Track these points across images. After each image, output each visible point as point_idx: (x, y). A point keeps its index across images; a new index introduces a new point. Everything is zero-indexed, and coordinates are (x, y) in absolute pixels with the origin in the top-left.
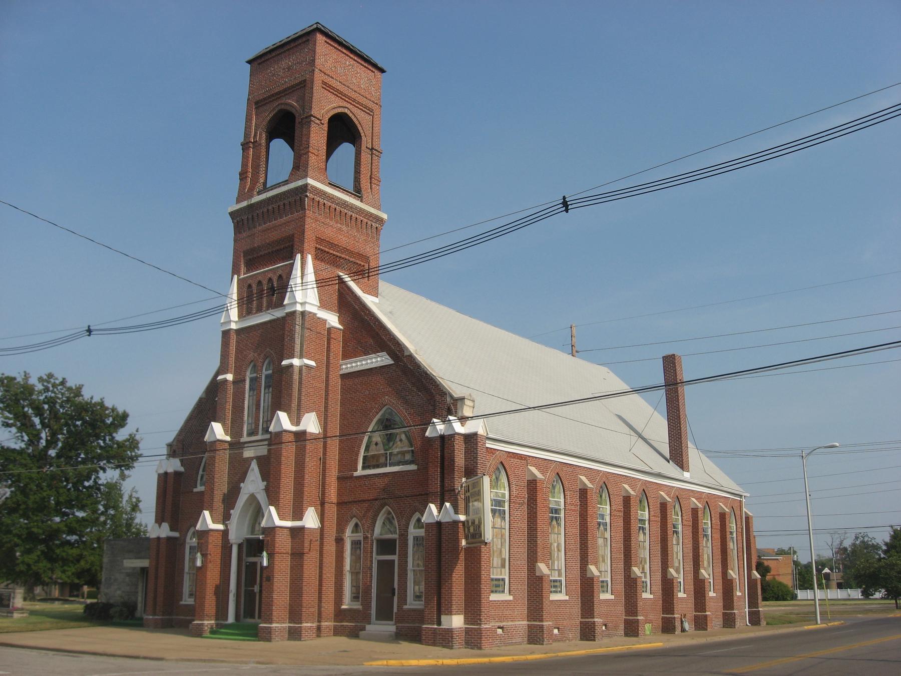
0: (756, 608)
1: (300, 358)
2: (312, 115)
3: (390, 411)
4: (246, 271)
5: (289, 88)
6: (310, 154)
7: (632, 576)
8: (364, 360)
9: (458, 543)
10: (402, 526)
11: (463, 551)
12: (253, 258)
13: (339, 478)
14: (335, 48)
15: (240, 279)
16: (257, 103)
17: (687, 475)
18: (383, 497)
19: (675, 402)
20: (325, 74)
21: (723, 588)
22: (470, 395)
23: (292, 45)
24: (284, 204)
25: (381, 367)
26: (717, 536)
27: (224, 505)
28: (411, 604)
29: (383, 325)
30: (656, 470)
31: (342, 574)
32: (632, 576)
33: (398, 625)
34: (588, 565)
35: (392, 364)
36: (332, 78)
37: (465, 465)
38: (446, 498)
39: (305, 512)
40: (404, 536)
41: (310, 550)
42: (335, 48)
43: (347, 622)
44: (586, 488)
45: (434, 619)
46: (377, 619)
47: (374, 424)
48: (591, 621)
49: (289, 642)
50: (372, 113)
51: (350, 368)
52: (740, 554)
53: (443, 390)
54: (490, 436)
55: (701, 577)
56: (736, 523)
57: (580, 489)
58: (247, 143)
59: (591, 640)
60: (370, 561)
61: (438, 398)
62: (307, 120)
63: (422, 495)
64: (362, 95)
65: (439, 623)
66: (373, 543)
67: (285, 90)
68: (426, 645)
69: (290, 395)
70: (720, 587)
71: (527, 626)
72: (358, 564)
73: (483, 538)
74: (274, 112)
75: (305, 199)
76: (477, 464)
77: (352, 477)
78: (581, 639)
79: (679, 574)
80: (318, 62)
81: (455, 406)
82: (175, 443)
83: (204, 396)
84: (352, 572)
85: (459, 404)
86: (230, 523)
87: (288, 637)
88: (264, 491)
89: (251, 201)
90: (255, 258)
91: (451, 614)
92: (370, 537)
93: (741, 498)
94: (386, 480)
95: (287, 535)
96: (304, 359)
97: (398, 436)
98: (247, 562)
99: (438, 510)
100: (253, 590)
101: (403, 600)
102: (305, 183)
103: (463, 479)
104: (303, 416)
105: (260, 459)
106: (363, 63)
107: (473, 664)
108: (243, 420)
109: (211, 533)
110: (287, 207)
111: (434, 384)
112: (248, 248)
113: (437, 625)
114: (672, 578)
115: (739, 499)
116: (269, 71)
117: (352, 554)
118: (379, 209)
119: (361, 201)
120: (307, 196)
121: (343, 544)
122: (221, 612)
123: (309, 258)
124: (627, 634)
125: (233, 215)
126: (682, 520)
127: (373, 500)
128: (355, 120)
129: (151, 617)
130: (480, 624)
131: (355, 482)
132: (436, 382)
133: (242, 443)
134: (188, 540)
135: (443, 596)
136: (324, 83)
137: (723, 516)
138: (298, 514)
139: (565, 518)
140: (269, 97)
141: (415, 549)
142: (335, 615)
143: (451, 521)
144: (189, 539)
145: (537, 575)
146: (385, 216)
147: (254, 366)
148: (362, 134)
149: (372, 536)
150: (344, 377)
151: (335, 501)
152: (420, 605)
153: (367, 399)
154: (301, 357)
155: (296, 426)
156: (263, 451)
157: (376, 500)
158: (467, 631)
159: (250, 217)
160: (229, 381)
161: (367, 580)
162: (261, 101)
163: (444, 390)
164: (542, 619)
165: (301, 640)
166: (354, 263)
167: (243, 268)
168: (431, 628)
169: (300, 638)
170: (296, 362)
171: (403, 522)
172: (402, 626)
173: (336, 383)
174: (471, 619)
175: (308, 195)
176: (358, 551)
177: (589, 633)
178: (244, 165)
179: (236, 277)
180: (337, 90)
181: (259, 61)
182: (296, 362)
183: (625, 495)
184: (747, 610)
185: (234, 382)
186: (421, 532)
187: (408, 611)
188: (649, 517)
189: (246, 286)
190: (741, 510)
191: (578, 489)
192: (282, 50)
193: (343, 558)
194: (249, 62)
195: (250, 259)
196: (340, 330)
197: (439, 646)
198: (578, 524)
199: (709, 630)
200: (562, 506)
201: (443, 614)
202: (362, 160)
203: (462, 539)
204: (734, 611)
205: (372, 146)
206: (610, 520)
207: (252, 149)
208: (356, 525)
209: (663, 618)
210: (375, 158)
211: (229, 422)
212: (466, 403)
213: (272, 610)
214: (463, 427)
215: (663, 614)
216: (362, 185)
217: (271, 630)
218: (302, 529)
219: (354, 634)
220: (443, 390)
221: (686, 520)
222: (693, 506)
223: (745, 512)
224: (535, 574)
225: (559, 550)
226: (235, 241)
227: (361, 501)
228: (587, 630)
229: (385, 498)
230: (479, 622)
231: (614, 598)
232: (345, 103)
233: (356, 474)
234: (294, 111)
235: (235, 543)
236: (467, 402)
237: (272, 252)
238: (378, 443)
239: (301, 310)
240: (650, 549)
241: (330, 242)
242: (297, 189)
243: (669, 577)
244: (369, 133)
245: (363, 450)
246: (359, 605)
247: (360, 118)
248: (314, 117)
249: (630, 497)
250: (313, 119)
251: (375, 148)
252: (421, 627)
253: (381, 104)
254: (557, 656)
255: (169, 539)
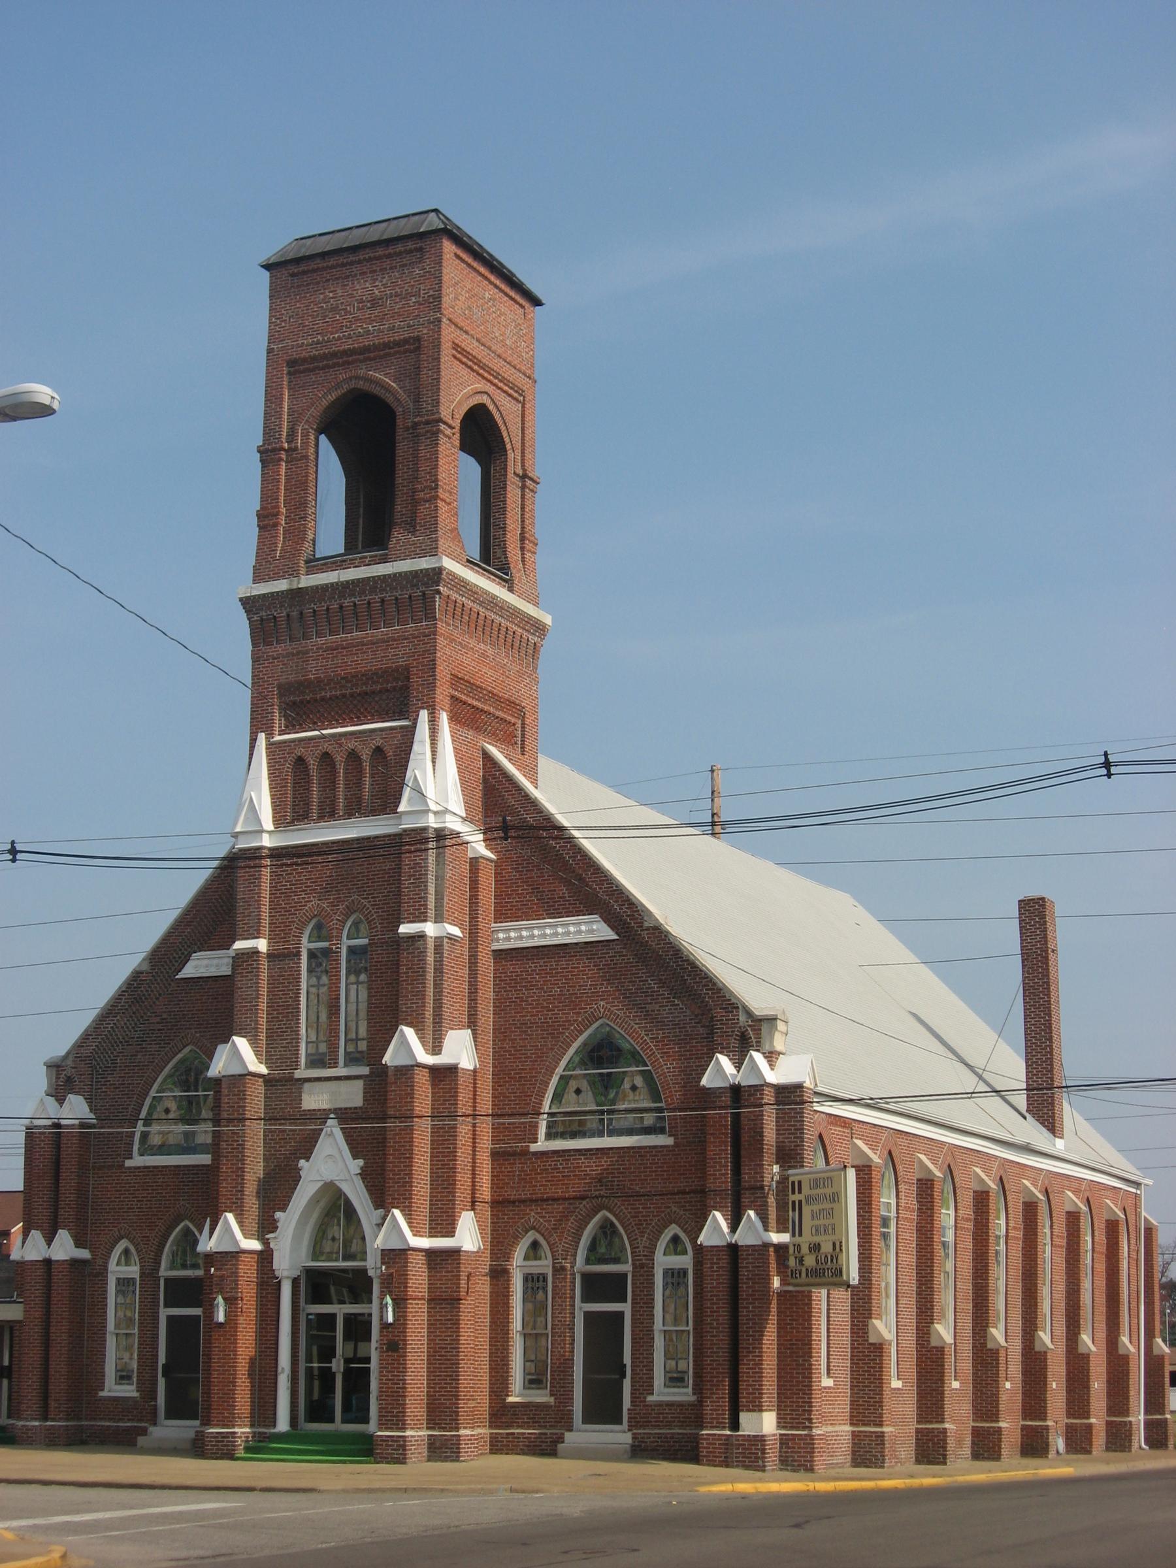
0: (1161, 1414)
1: (435, 922)
2: (440, 420)
3: (608, 1029)
4: (286, 727)
5: (376, 348)
6: (440, 504)
7: (990, 1345)
8: (550, 926)
9: (769, 1283)
10: (641, 1249)
11: (775, 1298)
12: (302, 702)
13: (495, 1155)
14: (469, 265)
15: (272, 744)
16: (292, 363)
17: (1060, 1144)
18: (597, 1193)
19: (1041, 996)
20: (456, 326)
21: (1108, 1373)
22: (784, 1012)
23: (380, 252)
24: (383, 601)
25: (586, 943)
26: (968, 1244)
27: (259, 1201)
28: (661, 1392)
29: (594, 862)
30: (1020, 1139)
31: (508, 1338)
32: (990, 1345)
33: (635, 1431)
34: (933, 1323)
35: (613, 940)
36: (466, 332)
37: (777, 1142)
38: (745, 1201)
39: (458, 1220)
40: (644, 1269)
41: (467, 1293)
42: (469, 265)
43: (519, 1427)
44: (931, 1178)
45: (725, 1419)
46: (585, 1421)
47: (573, 1052)
48: (938, 1429)
49: (430, 1463)
50: (522, 398)
51: (516, 938)
52: (1134, 1304)
53: (725, 996)
54: (820, 1089)
55: (1156, 1352)
56: (956, 1207)
57: (918, 1180)
58: (274, 450)
59: (938, 1463)
60: (570, 1313)
61: (718, 1013)
62: (428, 428)
63: (684, 1192)
64: (508, 363)
65: (735, 1425)
66: (575, 1279)
67: (366, 349)
68: (708, 1465)
69: (422, 995)
70: (911, 1364)
71: (850, 1433)
72: (541, 1319)
73: (845, 1277)
74: (339, 392)
75: (435, 597)
76: (803, 1141)
77: (525, 1152)
78: (918, 1461)
79: (1090, 1342)
80: (446, 301)
81: (758, 1032)
82: (69, 1062)
83: (145, 967)
84: (525, 1335)
85: (765, 1028)
86: (275, 1238)
87: (429, 1456)
88: (359, 1177)
89: (299, 583)
90: (309, 702)
91: (761, 1411)
92: (569, 1268)
93: (1137, 1189)
94: (605, 1162)
95: (422, 1264)
96: (446, 925)
97: (626, 1080)
98: (308, 1314)
99: (728, 1223)
100: (331, 1367)
101: (644, 1384)
102: (437, 565)
103: (775, 1166)
104: (446, 1035)
105: (344, 1115)
106: (507, 290)
107: (825, 1492)
108: (299, 1035)
109: (243, 1257)
110: (392, 609)
111: (710, 987)
112: (292, 678)
113: (729, 1430)
114: (1043, 1350)
115: (1134, 1190)
116: (322, 296)
117: (524, 1300)
118: (536, 604)
119: (511, 590)
120: (438, 592)
121: (509, 1281)
122: (263, 1411)
123: (444, 718)
124: (976, 1456)
125: (249, 604)
126: (1052, 1235)
127: (575, 1198)
128: (497, 416)
129: (37, 1423)
130: (810, 1428)
131: (533, 1163)
132: (714, 984)
133: (299, 1080)
134: (112, 1265)
135: (743, 1377)
136: (456, 346)
137: (926, 1187)
138: (444, 1224)
139: (897, 1235)
140: (324, 357)
141: (668, 1292)
142: (492, 1415)
143: (760, 1243)
144: (115, 1263)
145: (871, 1341)
146: (547, 619)
147: (319, 927)
148: (508, 446)
149: (572, 1267)
150: (499, 955)
151: (488, 1198)
152: (686, 1394)
153: (556, 1004)
154: (439, 919)
155: (433, 1054)
156: (352, 1095)
157: (583, 1198)
158: (784, 1441)
159: (295, 614)
160: (261, 953)
161: (564, 1348)
162: (304, 360)
163: (733, 1001)
164: (882, 1421)
165: (458, 1461)
166: (502, 719)
167: (278, 720)
168: (719, 1435)
169: (458, 1457)
170: (430, 929)
171: (644, 1242)
172: (644, 1434)
173: (487, 965)
174: (790, 1418)
175: (441, 589)
176: (540, 1295)
177: (933, 1451)
178: (268, 496)
179: (262, 737)
180: (473, 359)
181: (294, 269)
182: (430, 929)
183: (978, 1189)
184: (1142, 1417)
185: (270, 956)
186: (685, 1261)
187: (655, 1406)
188: (1007, 1230)
189: (291, 759)
190: (1137, 1214)
191: (1021, 1201)
192: (352, 258)
193: (508, 1307)
194: (267, 267)
195: (294, 703)
196: (491, 861)
197: (737, 1466)
198: (915, 1246)
199: (1094, 1453)
200: (893, 1214)
201: (743, 1411)
202: (509, 501)
203: (774, 1276)
204: (1130, 1419)
205: (524, 470)
206: (955, 1237)
207: (284, 464)
208: (535, 1245)
209: (1024, 1428)
210: (529, 495)
211: (263, 1036)
212: (778, 1028)
213: (405, 1404)
214: (772, 1072)
215: (1024, 1419)
216: (509, 555)
217: (405, 1441)
218: (455, 1253)
219: (547, 1448)
220: (730, 1000)
221: (1057, 1236)
222: (1069, 1207)
223: (1145, 1217)
224: (867, 1340)
225: (887, 1296)
226: (256, 659)
227: (547, 1200)
228: (930, 1445)
229: (602, 1197)
230: (807, 1424)
231: (958, 1387)
232: (495, 397)
233: (534, 1147)
234: (390, 399)
235: (288, 1277)
236: (781, 1026)
237: (352, 695)
238: (582, 1089)
239: (435, 826)
240: (1006, 1294)
241: (469, 683)
242: (415, 574)
243: (1037, 1349)
244: (517, 441)
245: (549, 1103)
246: (546, 1396)
247: (506, 411)
248: (445, 423)
249: (989, 1192)
250: (442, 426)
251: (530, 475)
252: (698, 1434)
253: (536, 378)
254: (956, 1482)
255: (74, 1263)
